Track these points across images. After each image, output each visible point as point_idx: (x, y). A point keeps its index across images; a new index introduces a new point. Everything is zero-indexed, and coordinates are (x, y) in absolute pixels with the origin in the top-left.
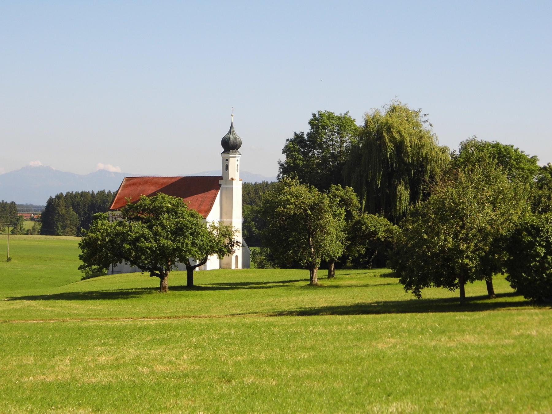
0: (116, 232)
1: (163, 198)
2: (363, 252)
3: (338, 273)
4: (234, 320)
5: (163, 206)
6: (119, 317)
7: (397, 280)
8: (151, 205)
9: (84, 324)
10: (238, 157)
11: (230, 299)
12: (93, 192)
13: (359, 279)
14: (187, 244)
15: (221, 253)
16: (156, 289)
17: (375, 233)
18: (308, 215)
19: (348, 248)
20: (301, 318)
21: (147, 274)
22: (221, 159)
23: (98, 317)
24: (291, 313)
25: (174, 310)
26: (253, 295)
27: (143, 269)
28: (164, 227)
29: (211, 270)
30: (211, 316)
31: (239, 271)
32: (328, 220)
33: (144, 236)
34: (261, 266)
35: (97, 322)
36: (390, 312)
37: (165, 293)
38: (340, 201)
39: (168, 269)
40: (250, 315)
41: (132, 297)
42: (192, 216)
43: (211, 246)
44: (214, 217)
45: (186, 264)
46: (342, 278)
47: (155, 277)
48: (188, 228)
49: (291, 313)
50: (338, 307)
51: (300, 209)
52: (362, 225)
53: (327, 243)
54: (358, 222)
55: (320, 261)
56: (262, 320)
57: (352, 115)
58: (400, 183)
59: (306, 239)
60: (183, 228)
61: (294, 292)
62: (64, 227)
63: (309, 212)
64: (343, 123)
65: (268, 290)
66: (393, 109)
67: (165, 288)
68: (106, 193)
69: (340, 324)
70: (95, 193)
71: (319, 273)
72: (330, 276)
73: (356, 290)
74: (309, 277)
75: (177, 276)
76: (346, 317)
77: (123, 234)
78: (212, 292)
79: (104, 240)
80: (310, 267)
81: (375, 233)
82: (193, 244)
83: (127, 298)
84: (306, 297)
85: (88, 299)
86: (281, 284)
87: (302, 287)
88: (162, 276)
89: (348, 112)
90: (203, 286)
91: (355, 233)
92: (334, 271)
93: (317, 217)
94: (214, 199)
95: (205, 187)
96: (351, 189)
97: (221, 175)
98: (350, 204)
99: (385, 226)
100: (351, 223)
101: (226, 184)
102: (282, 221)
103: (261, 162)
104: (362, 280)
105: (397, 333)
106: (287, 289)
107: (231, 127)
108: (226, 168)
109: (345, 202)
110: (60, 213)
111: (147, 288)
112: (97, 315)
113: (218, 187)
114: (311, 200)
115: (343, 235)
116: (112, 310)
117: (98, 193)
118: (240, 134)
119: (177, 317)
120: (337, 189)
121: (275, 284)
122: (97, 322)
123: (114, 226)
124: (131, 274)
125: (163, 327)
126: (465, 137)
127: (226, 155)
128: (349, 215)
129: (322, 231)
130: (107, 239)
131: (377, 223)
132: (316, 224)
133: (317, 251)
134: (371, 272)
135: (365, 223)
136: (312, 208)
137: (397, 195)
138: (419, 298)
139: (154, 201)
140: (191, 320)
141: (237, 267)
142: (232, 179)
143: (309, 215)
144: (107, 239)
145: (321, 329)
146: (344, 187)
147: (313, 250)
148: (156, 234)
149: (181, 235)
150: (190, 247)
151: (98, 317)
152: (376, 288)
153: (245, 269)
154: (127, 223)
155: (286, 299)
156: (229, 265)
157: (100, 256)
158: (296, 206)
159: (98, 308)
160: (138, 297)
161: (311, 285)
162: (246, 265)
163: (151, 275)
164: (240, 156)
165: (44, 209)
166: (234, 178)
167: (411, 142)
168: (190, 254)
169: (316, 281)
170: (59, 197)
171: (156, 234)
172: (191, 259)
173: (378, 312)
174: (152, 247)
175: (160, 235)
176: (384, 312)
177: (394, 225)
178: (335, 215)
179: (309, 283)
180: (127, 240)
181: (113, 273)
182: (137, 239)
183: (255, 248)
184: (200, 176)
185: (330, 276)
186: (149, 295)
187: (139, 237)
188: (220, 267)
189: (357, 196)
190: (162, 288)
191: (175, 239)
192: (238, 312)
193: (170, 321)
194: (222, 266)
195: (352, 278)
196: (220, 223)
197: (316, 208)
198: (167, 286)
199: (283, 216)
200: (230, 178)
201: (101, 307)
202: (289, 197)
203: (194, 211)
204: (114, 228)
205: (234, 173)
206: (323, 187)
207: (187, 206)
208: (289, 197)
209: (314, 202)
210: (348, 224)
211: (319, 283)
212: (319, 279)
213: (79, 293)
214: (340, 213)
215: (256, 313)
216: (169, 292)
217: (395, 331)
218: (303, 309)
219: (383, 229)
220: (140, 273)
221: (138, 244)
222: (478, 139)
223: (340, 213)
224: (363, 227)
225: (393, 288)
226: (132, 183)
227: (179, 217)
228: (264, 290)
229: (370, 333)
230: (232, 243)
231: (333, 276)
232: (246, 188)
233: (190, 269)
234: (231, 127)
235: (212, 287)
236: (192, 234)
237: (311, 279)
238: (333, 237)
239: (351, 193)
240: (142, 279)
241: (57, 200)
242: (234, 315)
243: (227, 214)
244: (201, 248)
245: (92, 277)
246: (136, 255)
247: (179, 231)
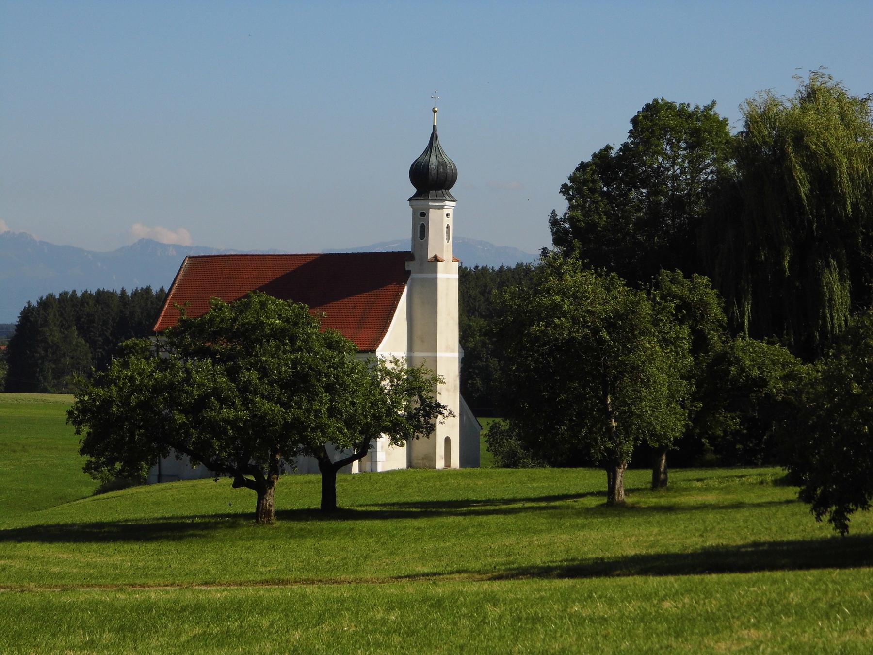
0: (153, 386)
1: (263, 305)
2: (732, 427)
3: (675, 476)
4: (411, 589)
5: (262, 323)
6: (151, 583)
7: (792, 492)
8: (234, 320)
9: (66, 599)
10: (449, 206)
11: (417, 540)
12: (123, 292)
13: (727, 490)
14: (318, 411)
15: (400, 431)
16: (247, 516)
17: (762, 382)
18: (601, 342)
19: (697, 419)
20: (567, 583)
21: (227, 481)
23: (102, 581)
24: (545, 572)
25: (281, 567)
26: (471, 531)
27: (216, 470)
28: (264, 372)
29: (388, 472)
30: (361, 581)
31: (455, 474)
32: (649, 352)
33: (216, 392)
34: (511, 461)
35: (96, 594)
36: (773, 567)
37: (268, 527)
38: (678, 308)
39: (276, 470)
40: (453, 576)
41: (190, 536)
42: (330, 346)
43: (374, 416)
44: (392, 348)
45: (319, 458)
46: (686, 489)
47: (245, 490)
48: (319, 373)
49: (545, 572)
50: (658, 557)
51: (583, 326)
52: (731, 364)
53: (646, 406)
54: (722, 359)
55: (632, 448)
56: (474, 587)
57: (721, 112)
58: (828, 265)
59: (598, 398)
60: (307, 374)
61: (567, 522)
62: (58, 374)
63: (605, 334)
65: (510, 519)
66: (811, 96)
67: (268, 513)
68: (154, 293)
69: (647, 597)
70: (129, 293)
71: (626, 478)
72: (658, 483)
73: (711, 516)
74: (605, 488)
75: (297, 487)
76: (671, 579)
77: (171, 387)
78: (377, 524)
79: (125, 402)
80: (610, 464)
81: (762, 382)
82: (332, 412)
83: (180, 538)
84: (593, 534)
85: (90, 541)
86: (543, 504)
87: (588, 512)
88: (262, 488)
90: (360, 509)
91: (715, 383)
92: (665, 473)
93: (624, 346)
94: (394, 307)
95: (376, 278)
96: (705, 280)
97: (408, 248)
98: (702, 316)
99: (783, 366)
100: (706, 359)
101: (421, 272)
102: (542, 355)
104: (729, 493)
105: (770, 617)
106: (552, 516)
107: (433, 137)
108: (421, 231)
109: (688, 312)
110: (50, 340)
111: (229, 515)
112: (103, 577)
114: (608, 307)
115: (685, 388)
116: (140, 564)
117: (135, 294)
118: (452, 151)
119: (281, 582)
120: (673, 281)
121: (527, 505)
122: (96, 594)
123: (149, 370)
124: (203, 481)
125: (238, 608)
127: (420, 203)
128: (700, 343)
129: (634, 380)
130: (134, 400)
131: (766, 359)
132: (622, 363)
133: (625, 426)
134: (753, 474)
135: (738, 360)
136: (610, 325)
137: (824, 295)
138: (842, 533)
139: (241, 312)
140: (310, 589)
142: (436, 259)
143: (605, 341)
144: (134, 400)
145: (601, 609)
146: (688, 276)
147: (614, 424)
148: (244, 389)
149: (304, 392)
150: (324, 419)
151: (102, 581)
152: (757, 511)
153: (468, 470)
154: (180, 364)
155: (545, 538)
156: (431, 458)
157: (122, 442)
158: (575, 320)
159: (111, 561)
160: (204, 536)
161: (612, 506)
162: (469, 458)
163: (235, 485)
164: (454, 204)
165: (13, 331)
166: (439, 255)
167: (850, 167)
168: (324, 434)
169: (621, 496)
170: (46, 304)
171: (244, 389)
172: (329, 447)
173: (745, 569)
174: (237, 419)
175: (255, 393)
176: (760, 568)
177: (804, 364)
178: (665, 342)
179: (604, 500)
180: (180, 404)
181: (160, 479)
182: (202, 403)
183: (497, 420)
184: (391, 251)
185: (658, 483)
186: (231, 531)
187: (207, 396)
189: (718, 296)
190: (260, 515)
191: (290, 399)
192: (426, 570)
193: (263, 592)
194: (415, 462)
195: (708, 489)
196: (409, 360)
197: (621, 324)
198: (273, 509)
199: (544, 344)
200: (430, 255)
201: (117, 559)
202: (558, 298)
203: (337, 335)
204: (150, 375)
205: (441, 244)
206: (639, 274)
207: (317, 324)
208: (558, 298)
209: (615, 311)
210: (697, 364)
211: (630, 500)
212: (628, 491)
213: (73, 525)
214: (678, 338)
215: (466, 571)
217: (769, 612)
218: (576, 563)
219: (779, 373)
220: (211, 481)
221: (208, 414)
223: (678, 338)
224: (733, 369)
225: (797, 510)
226: (203, 270)
227: (300, 349)
228: (501, 518)
229: (710, 617)
230: (433, 409)
231: (664, 482)
232: (464, 275)
233: (330, 471)
234: (433, 137)
235: (381, 512)
236: (329, 388)
237: (611, 491)
238: (660, 388)
239: (704, 290)
240: (217, 494)
241: (42, 312)
242: (411, 577)
243: (425, 341)
244: (350, 422)
245: (112, 489)
246: (199, 438)
247: (299, 383)
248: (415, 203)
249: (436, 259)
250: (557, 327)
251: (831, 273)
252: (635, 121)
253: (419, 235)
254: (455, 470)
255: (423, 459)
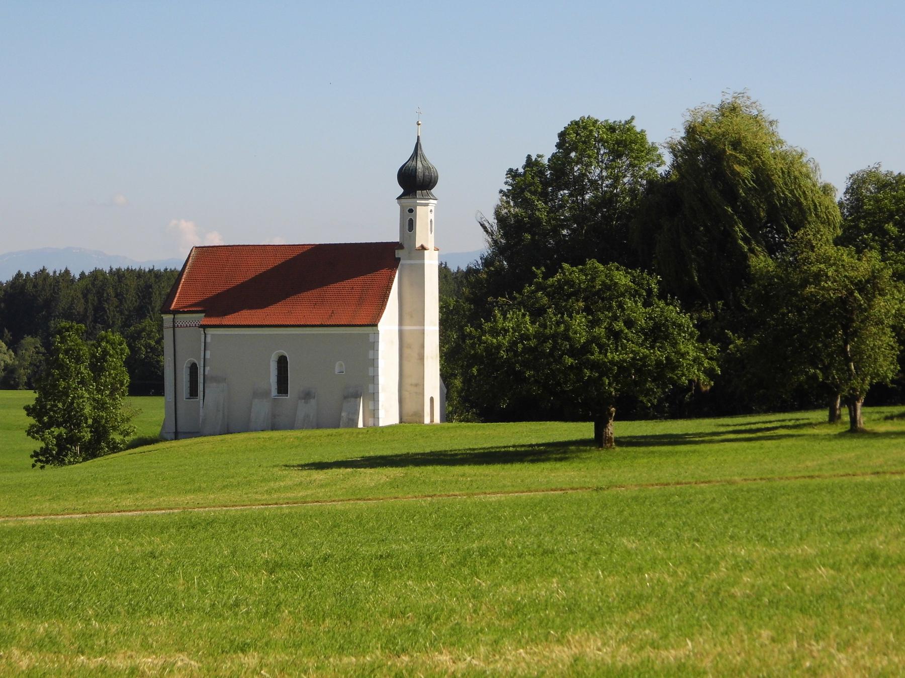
22: (397, 208)
64: (624, 142)
89: (633, 118)
94: (389, 288)
103: (454, 232)
107: (418, 146)
108: (409, 225)
113: (394, 263)
118: (435, 158)
126: (860, 165)
127: (408, 202)
141: (432, 421)
153: (447, 424)
164: (435, 202)
166: (425, 245)
188: (401, 421)
194: (404, 419)
200: (418, 245)
202: (822, 266)
205: (424, 235)
216: (618, 449)
222: (883, 170)
234: (418, 146)
248: (403, 201)
249: (423, 248)
250: (823, 288)
251: (757, 256)
252: (562, 135)
253: (407, 227)
254: (437, 425)
255: (412, 415)
